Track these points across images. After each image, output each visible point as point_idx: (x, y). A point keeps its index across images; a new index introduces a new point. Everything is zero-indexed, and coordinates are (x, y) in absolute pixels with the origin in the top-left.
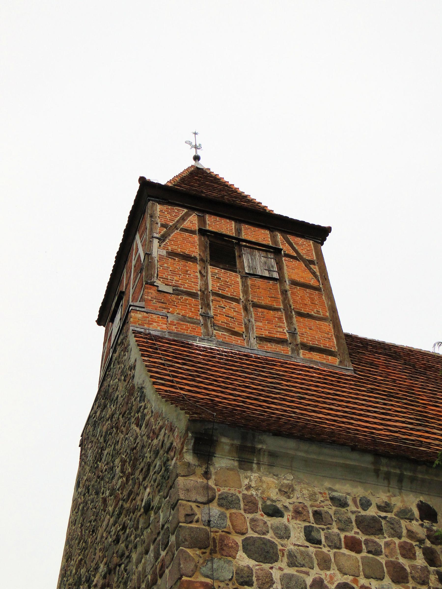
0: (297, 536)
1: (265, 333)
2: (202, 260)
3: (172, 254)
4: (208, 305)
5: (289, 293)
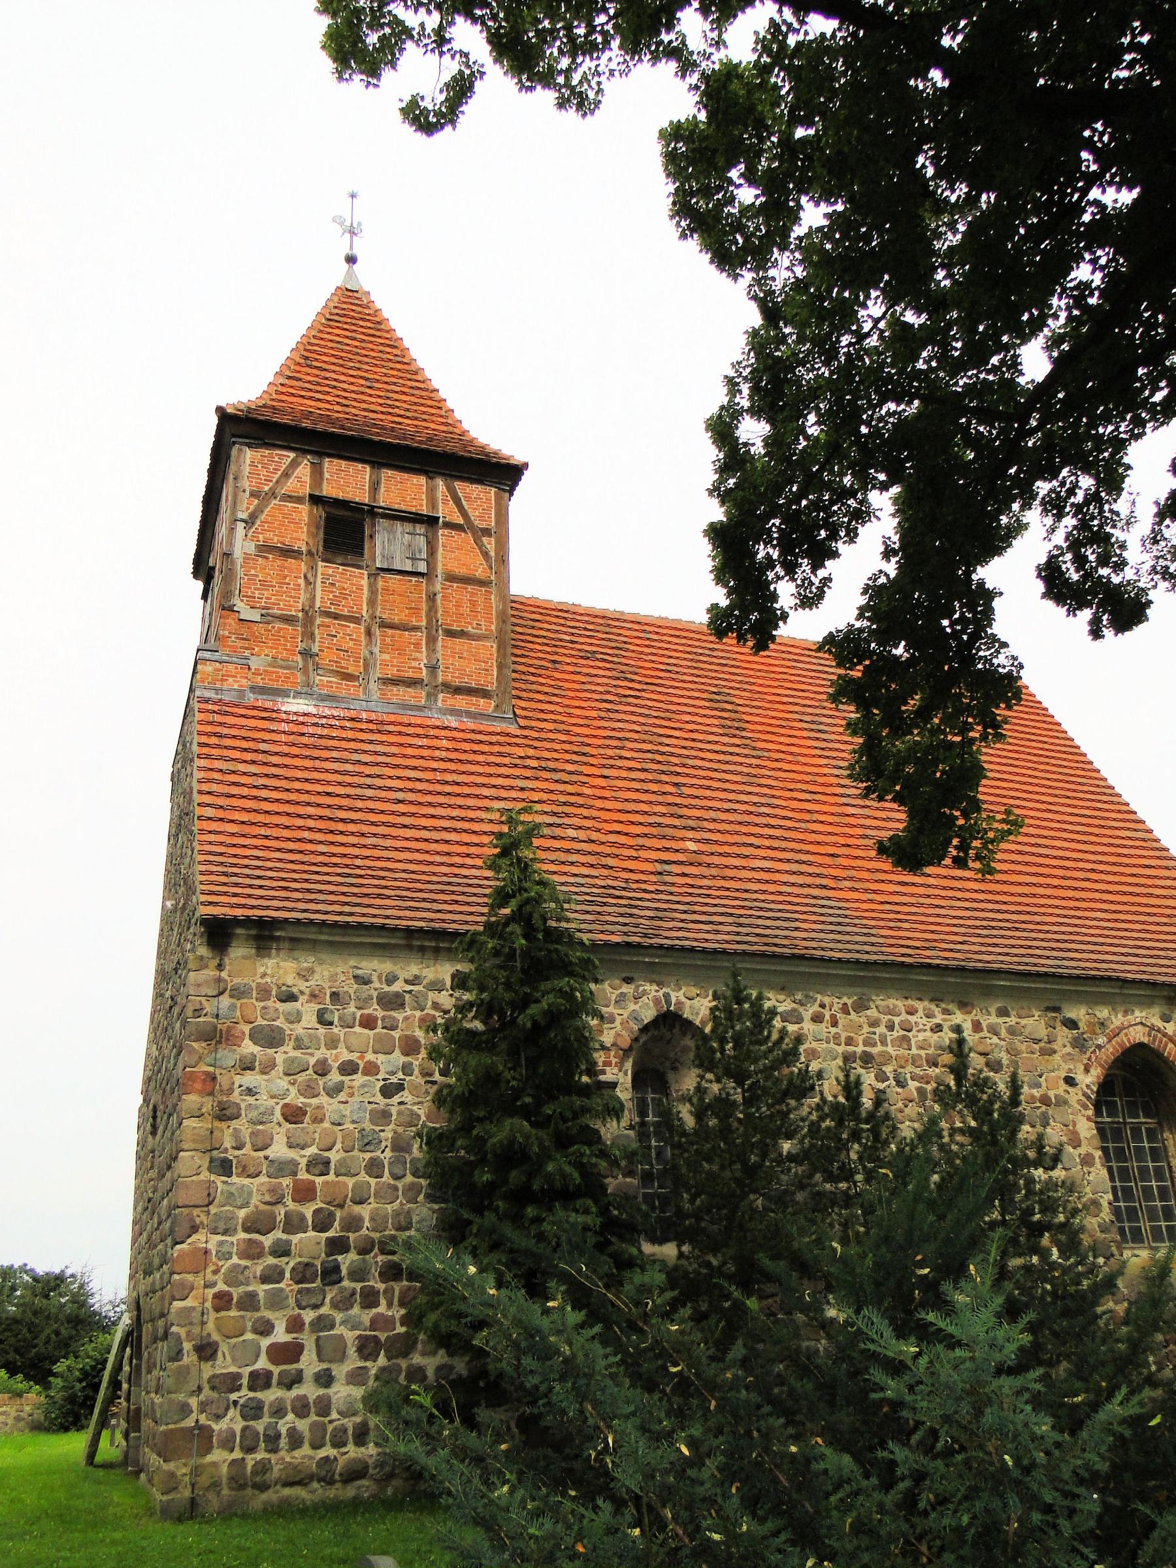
0: (309, 1018)
1: (392, 672)
2: (310, 553)
3: (265, 549)
4: (313, 634)
5: (439, 597)
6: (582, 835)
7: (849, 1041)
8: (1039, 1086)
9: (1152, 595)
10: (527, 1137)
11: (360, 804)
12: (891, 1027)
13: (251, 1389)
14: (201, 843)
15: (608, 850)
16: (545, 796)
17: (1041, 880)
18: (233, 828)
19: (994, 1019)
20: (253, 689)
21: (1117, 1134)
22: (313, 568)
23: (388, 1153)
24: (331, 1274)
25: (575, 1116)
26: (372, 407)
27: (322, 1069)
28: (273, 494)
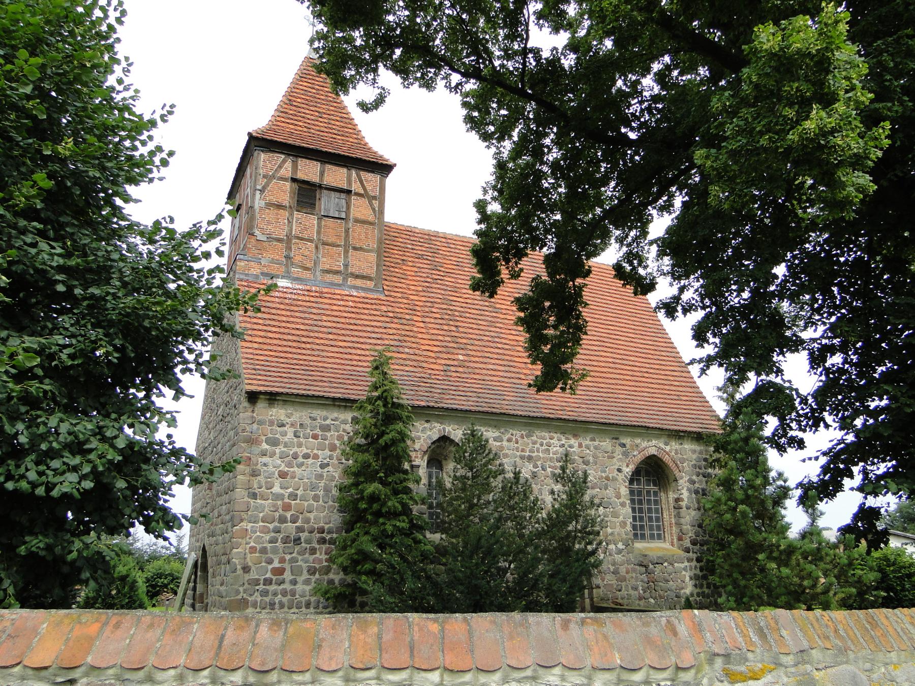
0: (290, 435)
1: (327, 267)
2: (290, 207)
3: (269, 205)
6: (411, 351)
7: (523, 450)
8: (605, 472)
9: (658, 280)
10: (380, 491)
11: (312, 334)
12: (542, 445)
13: (264, 585)
14: (243, 353)
15: (422, 359)
16: (395, 331)
17: (622, 377)
18: (256, 346)
19: (588, 442)
20: (262, 274)
21: (640, 493)
22: (292, 215)
23: (322, 492)
24: (297, 541)
25: (401, 482)
26: (322, 129)
27: (295, 456)
28: (273, 177)
